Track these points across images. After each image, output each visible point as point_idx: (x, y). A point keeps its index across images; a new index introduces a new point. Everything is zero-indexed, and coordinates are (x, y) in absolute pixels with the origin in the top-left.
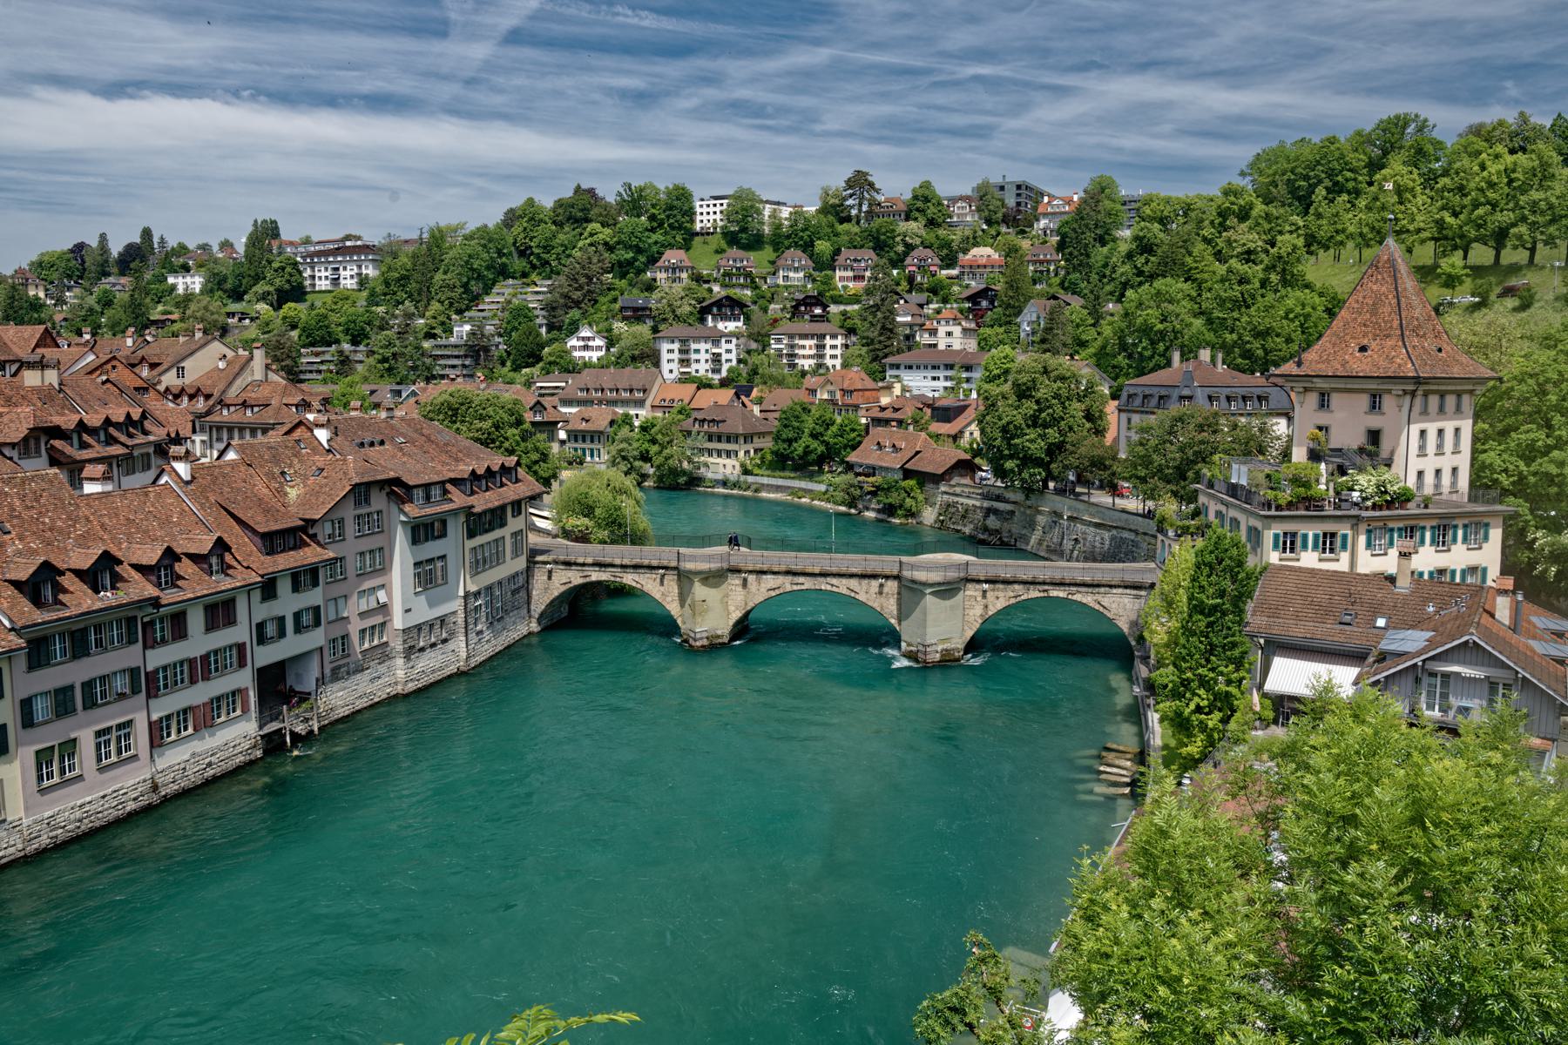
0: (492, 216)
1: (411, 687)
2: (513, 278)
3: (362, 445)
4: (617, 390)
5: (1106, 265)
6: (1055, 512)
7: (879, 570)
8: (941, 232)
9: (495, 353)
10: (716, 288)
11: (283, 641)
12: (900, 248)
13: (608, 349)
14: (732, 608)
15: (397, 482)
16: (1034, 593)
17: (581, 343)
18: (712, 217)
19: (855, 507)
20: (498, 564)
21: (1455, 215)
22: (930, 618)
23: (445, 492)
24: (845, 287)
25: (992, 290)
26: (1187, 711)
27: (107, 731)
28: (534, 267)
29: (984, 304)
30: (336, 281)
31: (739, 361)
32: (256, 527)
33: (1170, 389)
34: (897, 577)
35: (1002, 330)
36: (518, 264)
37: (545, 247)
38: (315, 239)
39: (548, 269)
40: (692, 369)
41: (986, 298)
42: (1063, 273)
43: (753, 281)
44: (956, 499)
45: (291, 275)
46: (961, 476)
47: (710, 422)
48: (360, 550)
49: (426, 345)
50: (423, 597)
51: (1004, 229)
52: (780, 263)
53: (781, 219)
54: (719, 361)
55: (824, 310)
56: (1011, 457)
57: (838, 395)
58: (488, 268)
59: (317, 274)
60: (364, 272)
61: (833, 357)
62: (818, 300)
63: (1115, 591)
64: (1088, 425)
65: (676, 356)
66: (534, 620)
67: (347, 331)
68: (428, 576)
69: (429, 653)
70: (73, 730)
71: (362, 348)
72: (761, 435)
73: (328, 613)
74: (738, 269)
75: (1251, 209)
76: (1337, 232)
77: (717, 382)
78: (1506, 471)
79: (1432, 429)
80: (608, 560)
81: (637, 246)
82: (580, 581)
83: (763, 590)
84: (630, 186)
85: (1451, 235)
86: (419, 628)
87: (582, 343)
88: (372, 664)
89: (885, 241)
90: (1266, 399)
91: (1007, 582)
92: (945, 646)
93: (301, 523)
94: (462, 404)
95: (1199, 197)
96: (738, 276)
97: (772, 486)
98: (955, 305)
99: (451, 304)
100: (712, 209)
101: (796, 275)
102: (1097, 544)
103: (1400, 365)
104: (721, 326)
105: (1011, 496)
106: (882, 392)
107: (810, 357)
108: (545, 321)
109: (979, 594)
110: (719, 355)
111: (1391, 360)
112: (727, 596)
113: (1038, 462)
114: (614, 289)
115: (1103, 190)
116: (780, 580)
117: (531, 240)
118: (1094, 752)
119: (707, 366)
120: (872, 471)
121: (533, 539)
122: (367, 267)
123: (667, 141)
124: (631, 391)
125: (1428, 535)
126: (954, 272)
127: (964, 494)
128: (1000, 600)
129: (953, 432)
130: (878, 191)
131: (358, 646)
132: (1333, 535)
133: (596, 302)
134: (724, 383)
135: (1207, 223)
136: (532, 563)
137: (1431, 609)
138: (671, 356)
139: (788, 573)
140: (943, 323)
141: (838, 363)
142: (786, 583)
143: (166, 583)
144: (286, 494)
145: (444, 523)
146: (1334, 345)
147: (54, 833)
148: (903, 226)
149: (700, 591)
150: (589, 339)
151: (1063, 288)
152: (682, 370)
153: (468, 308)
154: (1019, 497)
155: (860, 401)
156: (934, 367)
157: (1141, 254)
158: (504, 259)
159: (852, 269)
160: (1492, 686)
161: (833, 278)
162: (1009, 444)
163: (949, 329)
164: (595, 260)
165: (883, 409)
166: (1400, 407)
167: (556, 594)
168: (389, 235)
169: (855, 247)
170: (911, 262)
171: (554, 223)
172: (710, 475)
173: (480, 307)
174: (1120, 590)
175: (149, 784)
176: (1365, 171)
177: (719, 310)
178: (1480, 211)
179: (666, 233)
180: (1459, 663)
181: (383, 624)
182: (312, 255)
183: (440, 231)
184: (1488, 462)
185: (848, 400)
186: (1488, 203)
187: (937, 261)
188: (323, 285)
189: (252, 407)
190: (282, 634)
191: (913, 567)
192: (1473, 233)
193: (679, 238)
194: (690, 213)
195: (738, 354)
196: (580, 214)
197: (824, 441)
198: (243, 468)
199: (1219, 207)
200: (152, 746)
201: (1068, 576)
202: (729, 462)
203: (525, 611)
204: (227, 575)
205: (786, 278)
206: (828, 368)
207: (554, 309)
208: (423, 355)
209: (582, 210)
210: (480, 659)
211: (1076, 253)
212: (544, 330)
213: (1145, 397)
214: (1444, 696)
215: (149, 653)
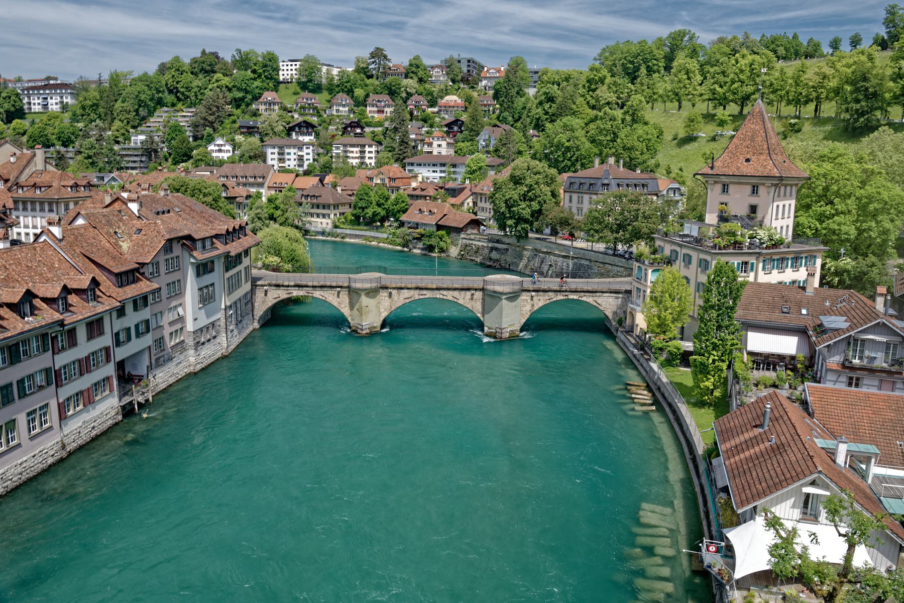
0: (151, 67)
1: (199, 367)
2: (166, 106)
3: (158, 213)
4: (246, 177)
5: (524, 108)
6: (536, 249)
7: (471, 286)
8: (427, 86)
9: (161, 154)
10: (296, 116)
11: (130, 343)
12: (404, 95)
13: (233, 152)
14: (382, 310)
15: (189, 237)
16: (560, 297)
17: (217, 148)
18: (290, 72)
19: (407, 247)
20: (239, 287)
21: (721, 87)
22: (504, 312)
23: (213, 243)
24: (373, 117)
25: (460, 120)
26: (678, 361)
27: (34, 411)
28: (179, 100)
29: (456, 128)
30: (45, 106)
31: (314, 160)
32: (111, 269)
33: (597, 180)
34: (483, 290)
35: (469, 144)
36: (169, 98)
37: (187, 88)
38: (25, 78)
39: (189, 102)
40: (286, 165)
41: (457, 125)
42: (498, 111)
43: (318, 112)
44: (471, 242)
45: (15, 102)
46: (472, 228)
47: (311, 196)
48: (168, 282)
49: (116, 147)
50: (203, 311)
51: (462, 86)
52: (334, 101)
53: (332, 75)
54: (302, 160)
55: (362, 130)
56: (511, 218)
57: (387, 181)
58: (151, 100)
59: (32, 102)
60: (65, 101)
61: (370, 158)
62: (358, 124)
63: (605, 295)
64: (554, 200)
65: (276, 156)
66: (256, 321)
67: (59, 139)
68: (206, 298)
69: (207, 346)
70: (14, 415)
71: (71, 149)
72: (343, 204)
73: (153, 325)
74: (309, 104)
75: (605, 79)
76: (654, 94)
77: (301, 172)
78: (810, 227)
79: (781, 204)
80: (304, 283)
81: (245, 89)
82: (286, 296)
85: (718, 98)
86: (201, 330)
87: (217, 148)
88: (176, 354)
89: (395, 90)
90: (647, 186)
91: (545, 291)
92: (512, 328)
93: (137, 266)
94: (182, 186)
95: (574, 70)
96: (309, 110)
97: (352, 235)
99: (128, 122)
100: (289, 68)
101: (344, 109)
102: (564, 267)
103: (770, 170)
104: (301, 138)
105: (506, 240)
106: (412, 179)
107: (356, 158)
108: (191, 134)
109: (529, 298)
110: (302, 156)
111: (765, 167)
112: (379, 303)
113: (526, 221)
114: (233, 115)
115: (518, 65)
116: (412, 292)
117: (178, 83)
118: (622, 387)
119: (295, 163)
120: (417, 226)
121: (255, 272)
122: (67, 98)
123: (207, 23)
124: (255, 177)
125: (790, 262)
126: (436, 110)
127: (476, 240)
129: (458, 203)
130: (389, 60)
131: (170, 343)
132: (746, 263)
133: (223, 122)
134: (307, 173)
135: (580, 86)
136: (254, 286)
137: (827, 304)
138: (273, 156)
139: (417, 288)
140: (436, 139)
141: (373, 161)
142: (416, 295)
143: (63, 309)
144: (121, 247)
145: (213, 262)
146: (731, 158)
147: (6, 484)
148: (405, 82)
149: (364, 300)
150: (222, 145)
151: (500, 121)
152: (280, 165)
153: (140, 125)
154: (513, 240)
155: (400, 185)
156: (434, 165)
157: (547, 102)
158: (160, 95)
159: (377, 106)
160: (888, 344)
161: (365, 111)
162: (510, 211)
163: (439, 143)
164: (221, 96)
165: (414, 189)
166: (769, 193)
167: (270, 304)
168: (81, 77)
169: (377, 93)
170: (411, 103)
171: (192, 73)
172: (313, 229)
173: (148, 125)
175: (60, 445)
176: (663, 60)
177: (300, 129)
178: (736, 85)
179: (263, 81)
180: (874, 334)
181: (182, 329)
182: (28, 89)
183: (117, 76)
184: (801, 222)
185: (393, 184)
186: (740, 81)
187: (426, 103)
188: (37, 108)
189: (22, 187)
190: (129, 339)
191: (493, 283)
192: (731, 97)
193: (271, 85)
194: (277, 70)
195: (314, 156)
196: (208, 68)
197: (385, 208)
198: (91, 230)
199: (588, 77)
200: (60, 419)
201: (579, 287)
202: (324, 220)
203: (251, 316)
204: (98, 302)
205: (338, 111)
206: (367, 165)
207: (197, 126)
208: (114, 154)
209: (210, 65)
210: (233, 347)
211: (506, 101)
212: (191, 139)
213: (581, 184)
214: (862, 351)
215: (56, 357)
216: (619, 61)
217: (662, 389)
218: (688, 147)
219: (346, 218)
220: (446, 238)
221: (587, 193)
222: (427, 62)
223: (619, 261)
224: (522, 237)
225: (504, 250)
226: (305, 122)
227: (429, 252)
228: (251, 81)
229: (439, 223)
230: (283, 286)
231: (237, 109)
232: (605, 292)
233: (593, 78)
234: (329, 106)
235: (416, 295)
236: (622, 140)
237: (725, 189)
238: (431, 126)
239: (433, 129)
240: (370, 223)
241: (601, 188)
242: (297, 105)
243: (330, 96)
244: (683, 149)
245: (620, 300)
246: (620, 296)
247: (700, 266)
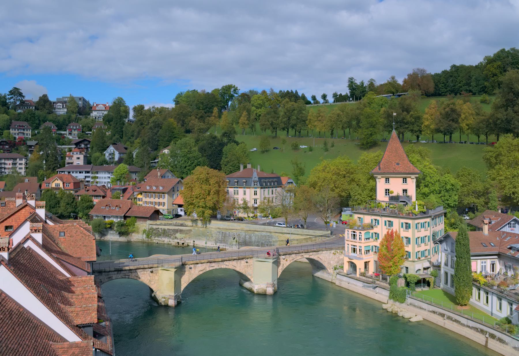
44: (157, 227)
91: (290, 254)
130: (23, 97)
163: (79, 156)
166: (413, 182)
222: (52, 98)
225: (188, 230)
229: (126, 215)
237: (387, 180)
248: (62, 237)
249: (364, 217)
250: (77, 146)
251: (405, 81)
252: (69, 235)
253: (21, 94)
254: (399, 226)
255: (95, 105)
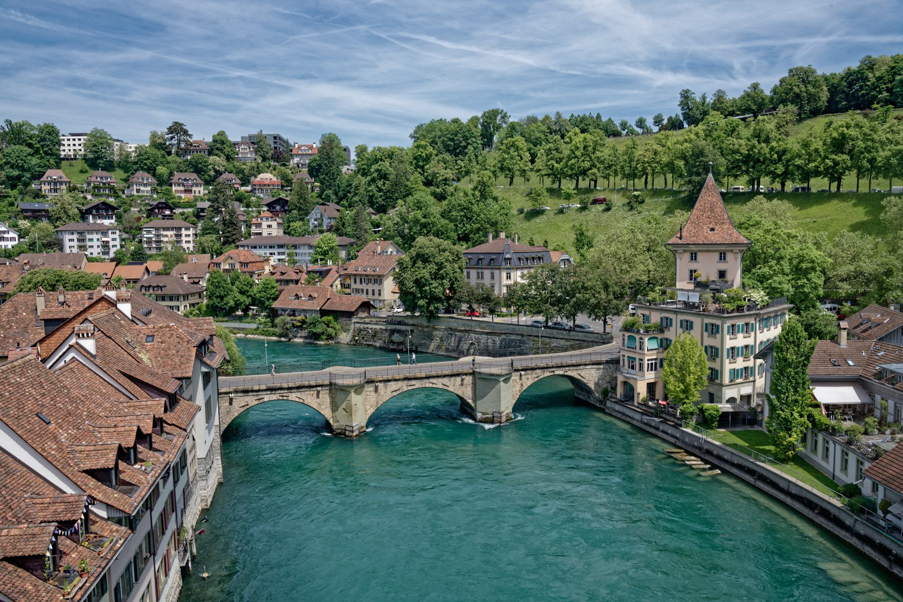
6: (451, 329)
7: (460, 371)
10: (89, 197)
12: (212, 173)
19: (286, 336)
24: (180, 198)
29: (278, 208)
34: (473, 374)
41: (279, 204)
43: (115, 192)
44: (366, 326)
47: (154, 287)
56: (422, 298)
57: (237, 266)
63: (587, 367)
65: (75, 243)
80: (278, 385)
81: (22, 166)
83: (389, 392)
84: (10, 123)
91: (533, 369)
98: (254, 209)
101: (145, 189)
102: (490, 344)
106: (265, 263)
109: (518, 378)
119: (99, 250)
120: (293, 313)
126: (249, 188)
128: (529, 380)
130: (190, 136)
141: (191, 246)
142: (404, 386)
155: (255, 269)
156: (271, 247)
157: (380, 180)
159: (183, 185)
163: (269, 223)
166: (736, 259)
169: (181, 171)
174: (590, 367)
176: (480, 138)
177: (97, 211)
178: (573, 161)
179: (42, 158)
187: (238, 181)
193: (52, 161)
194: (59, 143)
201: (566, 361)
205: (138, 191)
216: (439, 138)
217: (715, 452)
218: (538, 220)
219: (199, 309)
220: (334, 324)
221: (488, 268)
223: (558, 333)
224: (432, 316)
226: (104, 203)
227: (315, 340)
228: (29, 158)
230: (253, 391)
231: (12, 190)
232: (588, 365)
233: (420, 156)
234: (127, 185)
235: (404, 386)
236: (485, 214)
237: (694, 257)
238: (248, 206)
239: (250, 209)
240: (229, 313)
241: (503, 263)
242: (89, 184)
243: (126, 175)
244: (533, 221)
245: (601, 371)
246: (602, 367)
247: (706, 330)
248: (149, 344)
249: (650, 313)
250: (270, 208)
251: (774, 91)
252: (159, 340)
253: (186, 133)
254: (702, 329)
255: (297, 146)
